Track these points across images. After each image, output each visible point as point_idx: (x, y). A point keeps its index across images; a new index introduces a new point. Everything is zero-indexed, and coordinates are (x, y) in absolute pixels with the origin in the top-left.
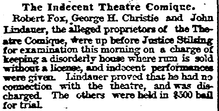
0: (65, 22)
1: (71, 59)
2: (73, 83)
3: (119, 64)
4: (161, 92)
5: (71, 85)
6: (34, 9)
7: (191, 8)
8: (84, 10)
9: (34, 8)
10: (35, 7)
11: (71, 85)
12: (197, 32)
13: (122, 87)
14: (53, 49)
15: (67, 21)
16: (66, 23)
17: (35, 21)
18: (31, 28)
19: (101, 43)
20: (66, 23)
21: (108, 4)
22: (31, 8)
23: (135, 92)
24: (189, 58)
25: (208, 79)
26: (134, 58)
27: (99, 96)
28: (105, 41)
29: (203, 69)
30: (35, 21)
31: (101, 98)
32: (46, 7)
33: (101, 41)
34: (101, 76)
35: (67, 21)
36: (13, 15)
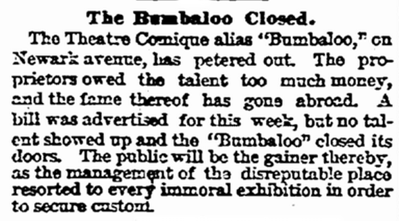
0: (294, 128)
1: (363, 192)
2: (292, 186)
3: (371, 185)
4: (330, 184)
5: (289, 188)
6: (108, 20)
7: (141, 63)
8: (40, 62)
9: (108, 19)
10: (110, 17)
11: (289, 188)
12: (88, 161)
13: (380, 194)
14: (123, 154)
15: (296, 126)
16: (295, 130)
17: (281, 125)
18: (148, 138)
19: (121, 145)
20: (295, 130)
21: (105, 12)
22: (102, 20)
23: (322, 185)
24: (45, 142)
25: (161, 161)
26: (182, 157)
27: (48, 158)
28: (127, 141)
29: (28, 158)
30: (281, 125)
31: (51, 161)
32: (130, 18)
33: (121, 141)
34: (380, 190)
35: (296, 126)
36: (391, 106)
